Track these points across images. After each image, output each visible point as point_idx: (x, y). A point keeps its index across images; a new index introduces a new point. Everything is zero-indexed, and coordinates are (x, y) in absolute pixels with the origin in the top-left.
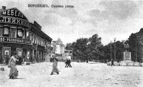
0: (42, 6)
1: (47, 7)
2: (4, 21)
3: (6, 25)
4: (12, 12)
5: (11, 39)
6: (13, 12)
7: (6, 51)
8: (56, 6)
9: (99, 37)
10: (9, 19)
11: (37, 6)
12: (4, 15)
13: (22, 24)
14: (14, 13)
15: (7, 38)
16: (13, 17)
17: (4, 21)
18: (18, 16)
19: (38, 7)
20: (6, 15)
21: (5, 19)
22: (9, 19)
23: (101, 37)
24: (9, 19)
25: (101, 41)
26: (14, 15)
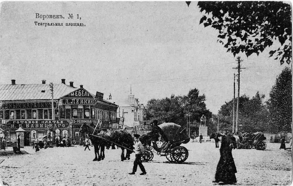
0: (56, 17)
1: (61, 18)
2: (73, 103)
3: (75, 106)
4: (79, 93)
5: (80, 121)
6: (80, 93)
7: (76, 133)
8: (81, 24)
9: (200, 94)
10: (77, 100)
11: (49, 17)
12: (73, 96)
13: (90, 100)
14: (81, 93)
15: (77, 120)
16: (81, 97)
17: (73, 103)
18: (85, 95)
19: (50, 18)
20: (75, 96)
21: (73, 100)
22: (78, 100)
23: (197, 89)
24: (78, 100)
25: (205, 102)
26: (81, 95)
